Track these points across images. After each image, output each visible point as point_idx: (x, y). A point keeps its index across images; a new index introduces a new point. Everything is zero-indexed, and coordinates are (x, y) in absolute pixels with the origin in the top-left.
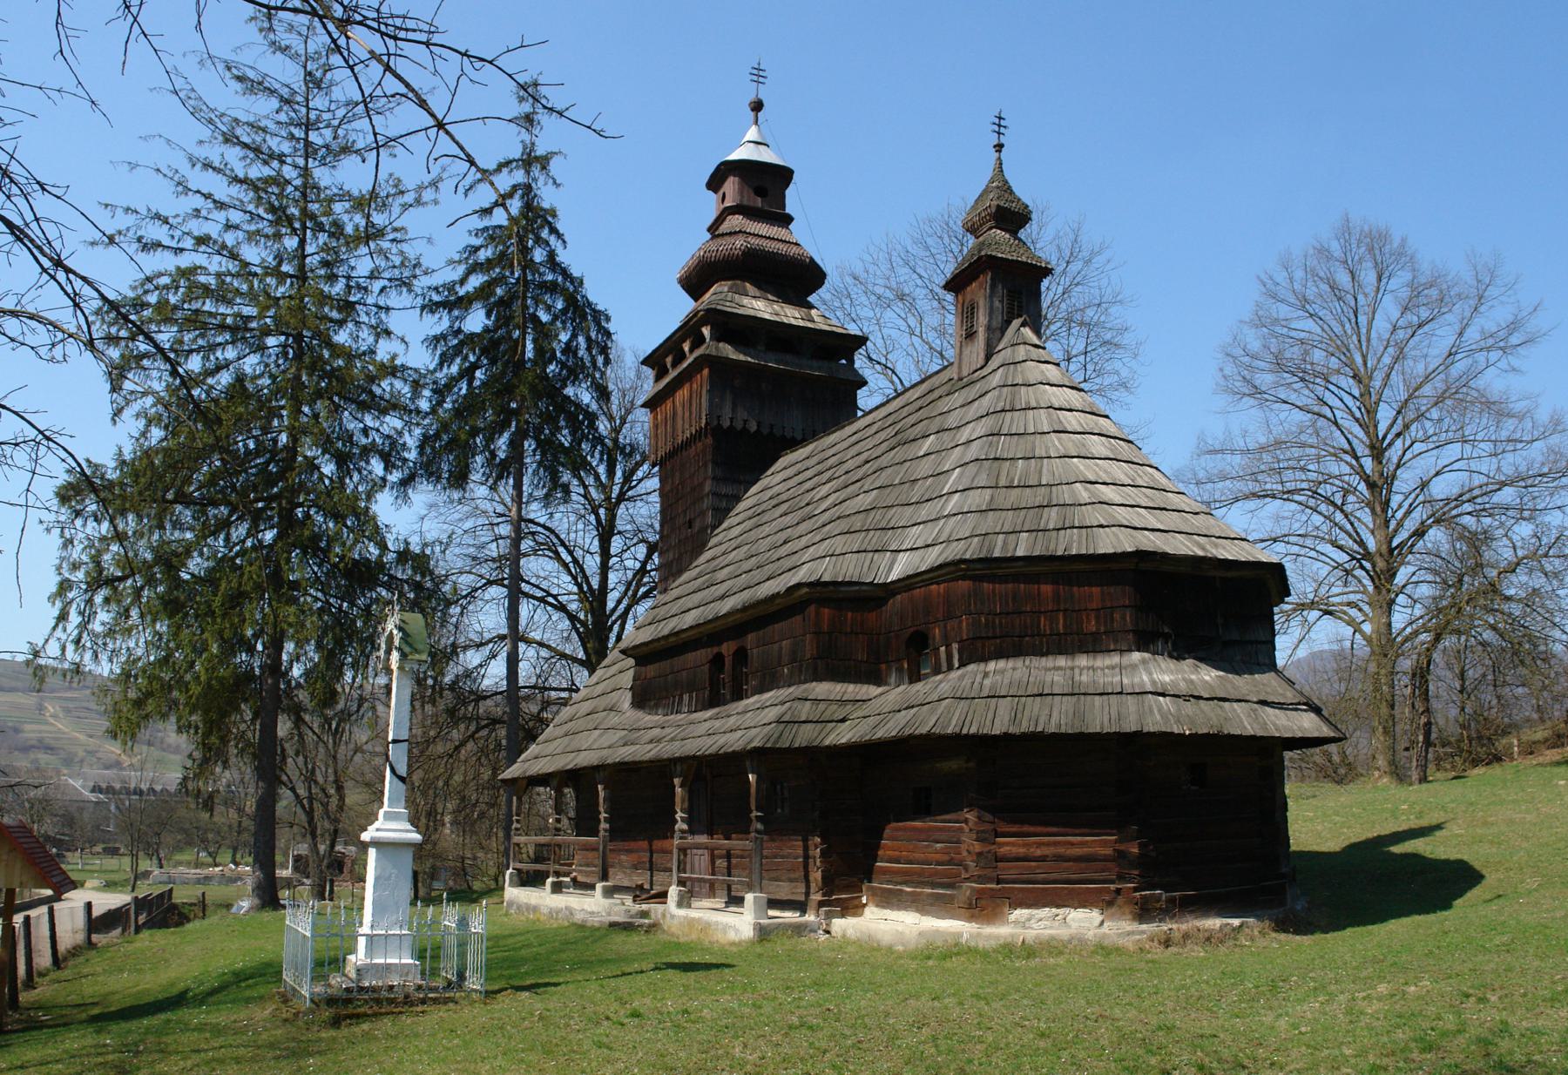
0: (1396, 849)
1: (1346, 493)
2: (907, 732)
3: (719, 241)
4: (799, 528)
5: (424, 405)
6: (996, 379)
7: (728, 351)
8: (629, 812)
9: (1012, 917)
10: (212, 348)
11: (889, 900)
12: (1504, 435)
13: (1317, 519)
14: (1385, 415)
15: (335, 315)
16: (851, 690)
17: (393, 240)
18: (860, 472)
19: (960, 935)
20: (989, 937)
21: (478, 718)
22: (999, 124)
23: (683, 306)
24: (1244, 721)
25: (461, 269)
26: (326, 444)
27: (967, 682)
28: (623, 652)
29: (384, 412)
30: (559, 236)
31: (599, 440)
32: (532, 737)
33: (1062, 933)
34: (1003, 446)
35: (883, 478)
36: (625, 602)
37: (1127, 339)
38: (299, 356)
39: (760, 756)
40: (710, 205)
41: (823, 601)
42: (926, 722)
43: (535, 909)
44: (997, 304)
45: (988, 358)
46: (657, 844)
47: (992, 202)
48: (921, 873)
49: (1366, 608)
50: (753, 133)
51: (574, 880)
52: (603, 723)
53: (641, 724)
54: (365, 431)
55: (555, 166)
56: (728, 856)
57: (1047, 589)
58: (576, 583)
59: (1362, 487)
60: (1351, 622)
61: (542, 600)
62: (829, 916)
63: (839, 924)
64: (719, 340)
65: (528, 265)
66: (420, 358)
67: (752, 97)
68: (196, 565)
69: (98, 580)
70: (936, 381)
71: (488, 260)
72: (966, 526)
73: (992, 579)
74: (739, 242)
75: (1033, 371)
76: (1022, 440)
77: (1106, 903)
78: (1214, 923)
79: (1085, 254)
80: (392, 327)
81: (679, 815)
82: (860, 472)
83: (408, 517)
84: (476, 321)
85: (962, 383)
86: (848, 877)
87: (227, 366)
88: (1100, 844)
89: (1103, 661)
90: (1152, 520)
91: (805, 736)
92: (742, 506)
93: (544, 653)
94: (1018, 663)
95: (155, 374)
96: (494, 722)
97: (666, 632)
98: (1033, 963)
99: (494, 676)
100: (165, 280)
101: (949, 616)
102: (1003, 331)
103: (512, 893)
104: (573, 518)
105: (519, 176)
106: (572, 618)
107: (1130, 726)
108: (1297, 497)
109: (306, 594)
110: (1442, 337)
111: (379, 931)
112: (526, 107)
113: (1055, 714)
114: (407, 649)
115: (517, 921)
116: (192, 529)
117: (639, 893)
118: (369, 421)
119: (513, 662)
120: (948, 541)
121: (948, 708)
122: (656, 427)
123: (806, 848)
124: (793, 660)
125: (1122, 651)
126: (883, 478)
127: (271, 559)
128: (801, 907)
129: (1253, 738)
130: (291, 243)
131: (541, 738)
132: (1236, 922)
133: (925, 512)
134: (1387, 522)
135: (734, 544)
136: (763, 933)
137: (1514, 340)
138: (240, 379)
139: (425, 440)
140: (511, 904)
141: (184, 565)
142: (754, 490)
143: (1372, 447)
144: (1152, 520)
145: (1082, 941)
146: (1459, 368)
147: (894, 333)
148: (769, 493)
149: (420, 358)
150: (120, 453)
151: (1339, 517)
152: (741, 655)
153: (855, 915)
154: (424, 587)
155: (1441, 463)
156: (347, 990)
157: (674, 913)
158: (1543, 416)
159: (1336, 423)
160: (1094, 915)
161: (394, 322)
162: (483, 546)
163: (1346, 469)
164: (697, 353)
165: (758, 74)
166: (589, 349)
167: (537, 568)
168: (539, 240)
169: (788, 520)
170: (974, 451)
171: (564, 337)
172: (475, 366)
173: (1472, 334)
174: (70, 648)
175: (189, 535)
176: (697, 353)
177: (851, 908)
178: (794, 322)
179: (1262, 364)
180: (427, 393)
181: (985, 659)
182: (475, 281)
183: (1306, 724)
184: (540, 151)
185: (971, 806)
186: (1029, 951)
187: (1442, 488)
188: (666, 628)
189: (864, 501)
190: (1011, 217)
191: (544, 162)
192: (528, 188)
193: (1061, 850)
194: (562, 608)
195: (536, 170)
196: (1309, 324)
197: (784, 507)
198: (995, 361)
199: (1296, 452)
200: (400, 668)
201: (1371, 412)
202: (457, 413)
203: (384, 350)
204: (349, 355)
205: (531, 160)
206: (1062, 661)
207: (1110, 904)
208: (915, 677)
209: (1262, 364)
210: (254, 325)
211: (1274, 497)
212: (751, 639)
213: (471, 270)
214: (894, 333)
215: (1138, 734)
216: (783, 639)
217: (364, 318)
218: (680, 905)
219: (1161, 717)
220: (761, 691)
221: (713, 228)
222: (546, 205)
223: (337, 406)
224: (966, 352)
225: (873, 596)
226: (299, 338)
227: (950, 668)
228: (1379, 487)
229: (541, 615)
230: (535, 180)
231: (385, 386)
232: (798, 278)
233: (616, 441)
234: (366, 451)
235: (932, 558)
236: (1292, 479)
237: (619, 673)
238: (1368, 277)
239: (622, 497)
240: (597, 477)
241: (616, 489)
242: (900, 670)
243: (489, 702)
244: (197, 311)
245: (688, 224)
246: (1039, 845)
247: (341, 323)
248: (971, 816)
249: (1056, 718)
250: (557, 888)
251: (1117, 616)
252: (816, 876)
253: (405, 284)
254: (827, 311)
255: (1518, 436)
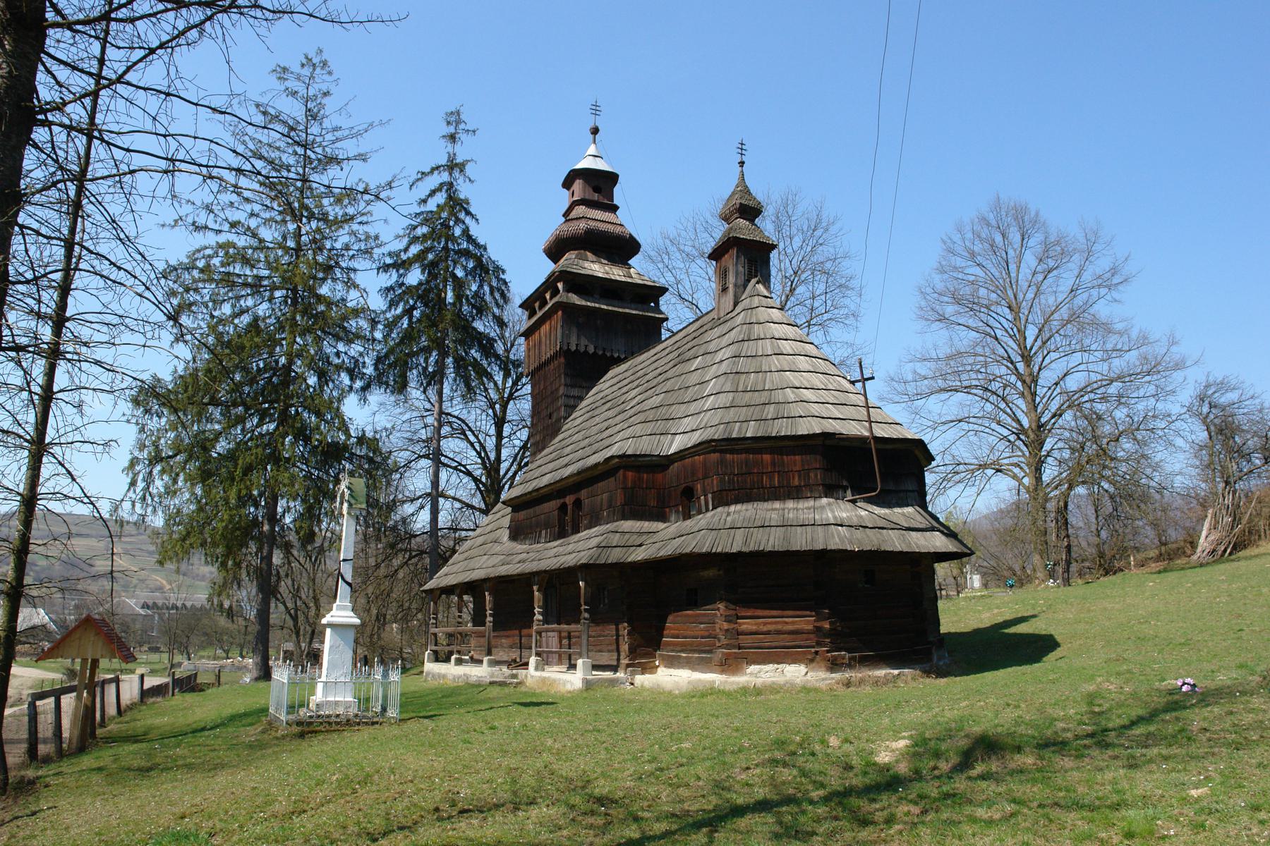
0: (1012, 630)
1: (1005, 387)
2: (679, 551)
3: (569, 224)
4: (626, 416)
5: (378, 335)
6: (739, 319)
7: (575, 299)
8: (508, 609)
9: (748, 671)
10: (238, 298)
11: (672, 663)
12: (1109, 346)
13: (989, 407)
14: (1031, 333)
15: (321, 275)
16: (646, 525)
17: (360, 223)
18: (655, 381)
19: (714, 682)
20: (733, 683)
21: (410, 550)
22: (742, 148)
23: (547, 267)
24: (895, 542)
25: (406, 240)
26: (311, 365)
27: (716, 518)
28: (504, 503)
29: (349, 342)
30: (473, 216)
31: (497, 357)
32: (446, 560)
33: (780, 680)
34: (742, 364)
35: (668, 386)
36: (513, 469)
37: (854, 283)
38: (295, 302)
39: (585, 568)
40: (564, 199)
41: (626, 468)
42: (690, 545)
43: (444, 676)
44: (741, 269)
45: (736, 304)
46: (525, 632)
47: (737, 201)
48: (691, 644)
49: (1026, 468)
50: (592, 150)
51: (472, 658)
52: (491, 551)
53: (514, 551)
54: (338, 354)
55: (469, 169)
56: (569, 637)
57: (767, 457)
58: (480, 457)
59: (1019, 384)
60: (1014, 477)
61: (455, 468)
62: (633, 674)
63: (640, 679)
64: (568, 291)
65: (450, 238)
66: (377, 303)
67: (592, 125)
68: (222, 446)
69: (156, 459)
70: (705, 319)
71: (424, 235)
72: (716, 418)
73: (732, 452)
74: (582, 225)
75: (763, 314)
76: (754, 360)
77: (810, 661)
78: (881, 672)
79: (824, 224)
80: (358, 282)
81: (537, 610)
82: (655, 381)
83: (365, 413)
84: (415, 276)
85: (719, 322)
86: (646, 646)
87: (247, 311)
88: (805, 622)
89: (802, 504)
90: (835, 412)
91: (615, 556)
92: (584, 403)
93: (457, 505)
94: (749, 506)
95: (200, 316)
96: (422, 552)
97: (530, 489)
98: (759, 698)
99: (422, 521)
100: (209, 252)
101: (705, 477)
102: (745, 287)
103: (430, 667)
104: (479, 412)
105: (445, 177)
106: (476, 480)
107: (819, 546)
108: (974, 391)
109: (294, 465)
110: (1066, 279)
111: (333, 685)
112: (452, 129)
113: (772, 539)
114: (353, 501)
115: (432, 684)
116: (219, 422)
117: (512, 664)
118: (341, 347)
119: (435, 512)
120: (705, 427)
121: (704, 536)
122: (529, 350)
123: (617, 630)
124: (610, 506)
125: (815, 498)
126: (668, 386)
127: (272, 441)
128: (614, 669)
129: (901, 552)
130: (292, 227)
131: (451, 562)
132: (896, 672)
133: (693, 408)
134: (1036, 408)
135: (577, 429)
136: (588, 685)
137: (1115, 281)
138: (256, 319)
139: (379, 361)
140: (428, 674)
141: (214, 447)
142: (591, 393)
143: (1022, 356)
144: (835, 412)
145: (793, 685)
146: (1079, 301)
147: (698, 279)
148: (602, 395)
149: (377, 303)
150: (176, 371)
151: (1003, 405)
152: (578, 503)
153: (651, 673)
154: (374, 462)
155: (1071, 365)
156: (311, 717)
157: (534, 675)
158: (1134, 334)
159: (996, 339)
160: (802, 669)
161: (359, 278)
162: (415, 432)
163: (1003, 370)
164: (555, 300)
165: (596, 109)
166: (492, 293)
167: (452, 446)
168: (458, 221)
169: (610, 413)
170: (724, 367)
171: (474, 288)
172: (413, 308)
173: (1087, 276)
174: (138, 505)
175: (217, 427)
176: (555, 300)
177: (648, 669)
178: (618, 278)
179: (946, 299)
180: (380, 327)
181: (728, 504)
182: (414, 250)
183: (938, 544)
184: (459, 160)
185: (721, 600)
186: (758, 691)
187: (1072, 383)
188: (530, 487)
189: (656, 401)
190: (750, 211)
191: (461, 167)
192: (451, 185)
193: (780, 627)
194: (468, 473)
195: (456, 173)
196: (978, 271)
197: (609, 405)
198: (739, 309)
199: (971, 360)
200: (349, 513)
201: (1022, 333)
202: (402, 342)
203: (353, 299)
204: (329, 303)
205: (453, 166)
206: (777, 505)
207: (812, 661)
208: (687, 516)
209: (946, 299)
210: (265, 283)
211: (956, 391)
212: (583, 494)
213: (414, 240)
214: (698, 279)
215: (824, 552)
216: (603, 493)
217: (339, 275)
218: (537, 669)
219: (839, 540)
220: (590, 528)
221: (566, 214)
222: (462, 196)
223: (319, 337)
224: (722, 301)
225: (662, 463)
226: (295, 291)
227: (707, 510)
228: (1030, 382)
229: (454, 478)
230: (456, 180)
231: (352, 324)
232: (621, 248)
233: (508, 357)
234: (339, 368)
235: (695, 438)
236: (966, 379)
237: (502, 517)
238: (1015, 237)
239: (511, 397)
240: (496, 384)
241: (507, 391)
242: (677, 512)
243: (418, 539)
244: (228, 274)
245: (549, 211)
246: (765, 624)
247: (324, 280)
248: (721, 606)
249: (772, 541)
250: (459, 662)
251: (812, 475)
252: (625, 648)
253: (368, 252)
254: (641, 269)
255: (1119, 347)
